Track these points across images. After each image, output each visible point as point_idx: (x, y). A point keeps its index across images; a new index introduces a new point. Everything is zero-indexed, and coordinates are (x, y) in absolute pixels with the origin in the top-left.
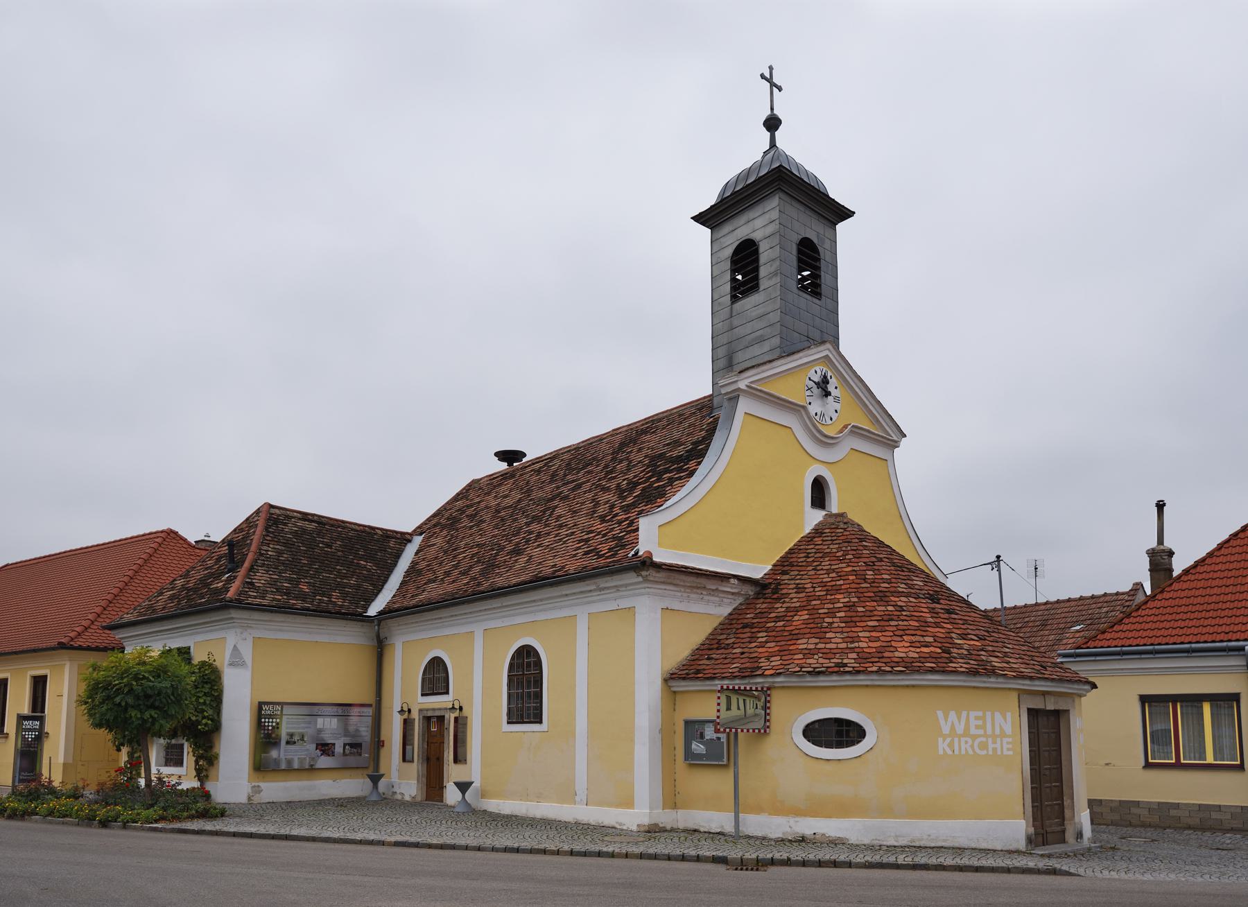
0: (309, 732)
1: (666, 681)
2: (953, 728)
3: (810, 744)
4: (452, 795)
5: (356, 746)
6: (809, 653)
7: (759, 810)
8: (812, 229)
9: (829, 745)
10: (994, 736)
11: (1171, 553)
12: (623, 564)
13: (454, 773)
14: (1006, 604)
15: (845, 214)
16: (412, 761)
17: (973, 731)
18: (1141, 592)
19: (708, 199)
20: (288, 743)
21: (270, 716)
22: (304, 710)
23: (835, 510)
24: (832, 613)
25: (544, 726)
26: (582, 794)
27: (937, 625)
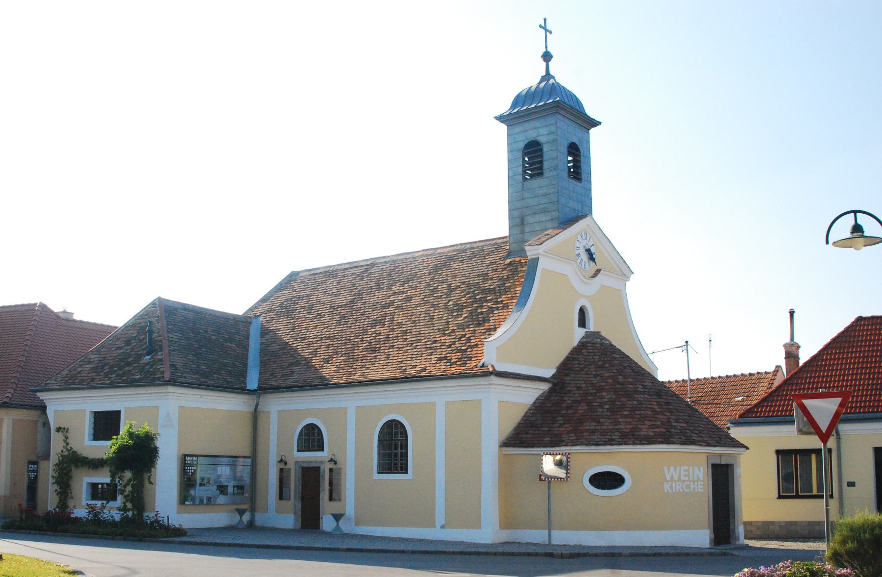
0: (213, 477)
1: (500, 447)
2: (672, 477)
3: (593, 487)
4: (327, 523)
5: (241, 488)
6: (593, 432)
7: (562, 528)
8: (573, 134)
9: (603, 488)
10: (694, 481)
11: (798, 347)
12: (467, 368)
13: (327, 508)
14: (692, 378)
15: (594, 123)
16: (289, 499)
17: (683, 478)
18: (779, 374)
19: (504, 107)
20: (201, 485)
21: (190, 465)
22: (211, 460)
23: (592, 330)
24: (601, 405)
25: (409, 476)
26: (440, 519)
27: (662, 413)
